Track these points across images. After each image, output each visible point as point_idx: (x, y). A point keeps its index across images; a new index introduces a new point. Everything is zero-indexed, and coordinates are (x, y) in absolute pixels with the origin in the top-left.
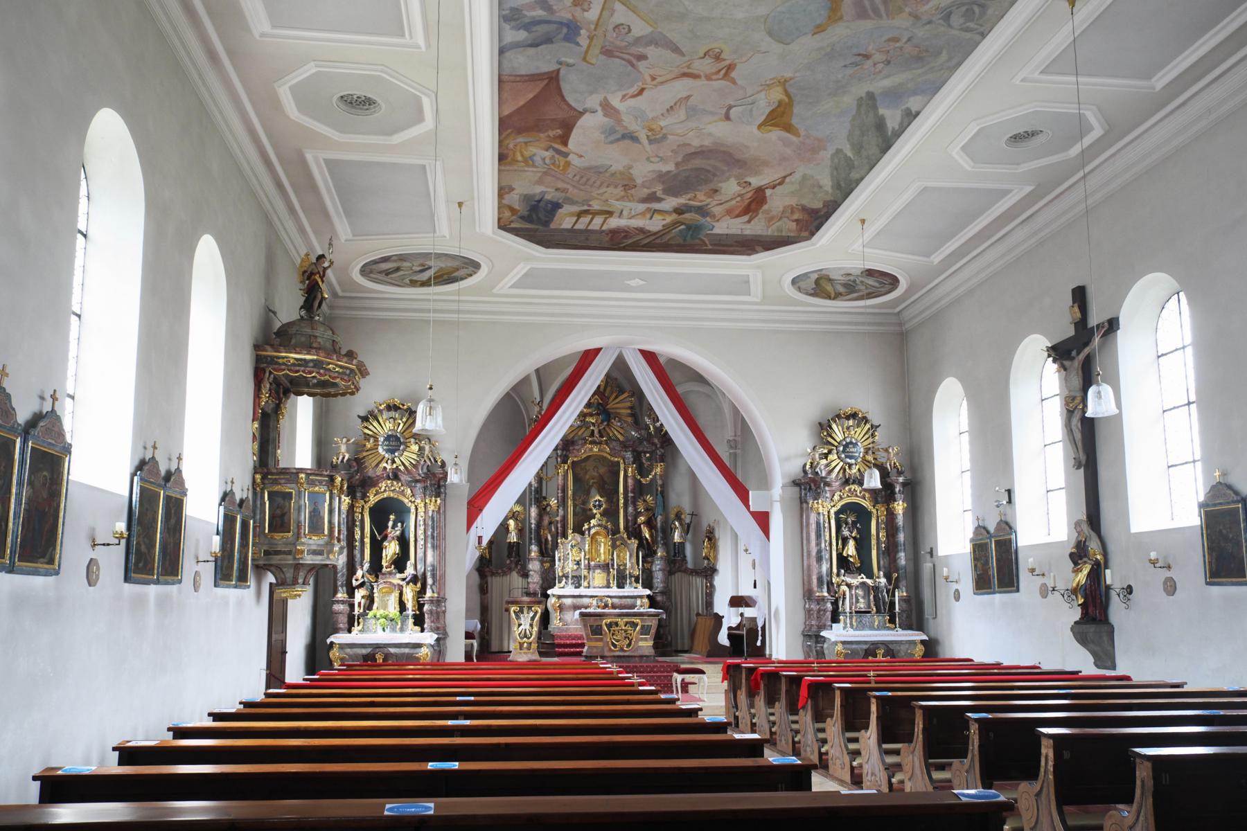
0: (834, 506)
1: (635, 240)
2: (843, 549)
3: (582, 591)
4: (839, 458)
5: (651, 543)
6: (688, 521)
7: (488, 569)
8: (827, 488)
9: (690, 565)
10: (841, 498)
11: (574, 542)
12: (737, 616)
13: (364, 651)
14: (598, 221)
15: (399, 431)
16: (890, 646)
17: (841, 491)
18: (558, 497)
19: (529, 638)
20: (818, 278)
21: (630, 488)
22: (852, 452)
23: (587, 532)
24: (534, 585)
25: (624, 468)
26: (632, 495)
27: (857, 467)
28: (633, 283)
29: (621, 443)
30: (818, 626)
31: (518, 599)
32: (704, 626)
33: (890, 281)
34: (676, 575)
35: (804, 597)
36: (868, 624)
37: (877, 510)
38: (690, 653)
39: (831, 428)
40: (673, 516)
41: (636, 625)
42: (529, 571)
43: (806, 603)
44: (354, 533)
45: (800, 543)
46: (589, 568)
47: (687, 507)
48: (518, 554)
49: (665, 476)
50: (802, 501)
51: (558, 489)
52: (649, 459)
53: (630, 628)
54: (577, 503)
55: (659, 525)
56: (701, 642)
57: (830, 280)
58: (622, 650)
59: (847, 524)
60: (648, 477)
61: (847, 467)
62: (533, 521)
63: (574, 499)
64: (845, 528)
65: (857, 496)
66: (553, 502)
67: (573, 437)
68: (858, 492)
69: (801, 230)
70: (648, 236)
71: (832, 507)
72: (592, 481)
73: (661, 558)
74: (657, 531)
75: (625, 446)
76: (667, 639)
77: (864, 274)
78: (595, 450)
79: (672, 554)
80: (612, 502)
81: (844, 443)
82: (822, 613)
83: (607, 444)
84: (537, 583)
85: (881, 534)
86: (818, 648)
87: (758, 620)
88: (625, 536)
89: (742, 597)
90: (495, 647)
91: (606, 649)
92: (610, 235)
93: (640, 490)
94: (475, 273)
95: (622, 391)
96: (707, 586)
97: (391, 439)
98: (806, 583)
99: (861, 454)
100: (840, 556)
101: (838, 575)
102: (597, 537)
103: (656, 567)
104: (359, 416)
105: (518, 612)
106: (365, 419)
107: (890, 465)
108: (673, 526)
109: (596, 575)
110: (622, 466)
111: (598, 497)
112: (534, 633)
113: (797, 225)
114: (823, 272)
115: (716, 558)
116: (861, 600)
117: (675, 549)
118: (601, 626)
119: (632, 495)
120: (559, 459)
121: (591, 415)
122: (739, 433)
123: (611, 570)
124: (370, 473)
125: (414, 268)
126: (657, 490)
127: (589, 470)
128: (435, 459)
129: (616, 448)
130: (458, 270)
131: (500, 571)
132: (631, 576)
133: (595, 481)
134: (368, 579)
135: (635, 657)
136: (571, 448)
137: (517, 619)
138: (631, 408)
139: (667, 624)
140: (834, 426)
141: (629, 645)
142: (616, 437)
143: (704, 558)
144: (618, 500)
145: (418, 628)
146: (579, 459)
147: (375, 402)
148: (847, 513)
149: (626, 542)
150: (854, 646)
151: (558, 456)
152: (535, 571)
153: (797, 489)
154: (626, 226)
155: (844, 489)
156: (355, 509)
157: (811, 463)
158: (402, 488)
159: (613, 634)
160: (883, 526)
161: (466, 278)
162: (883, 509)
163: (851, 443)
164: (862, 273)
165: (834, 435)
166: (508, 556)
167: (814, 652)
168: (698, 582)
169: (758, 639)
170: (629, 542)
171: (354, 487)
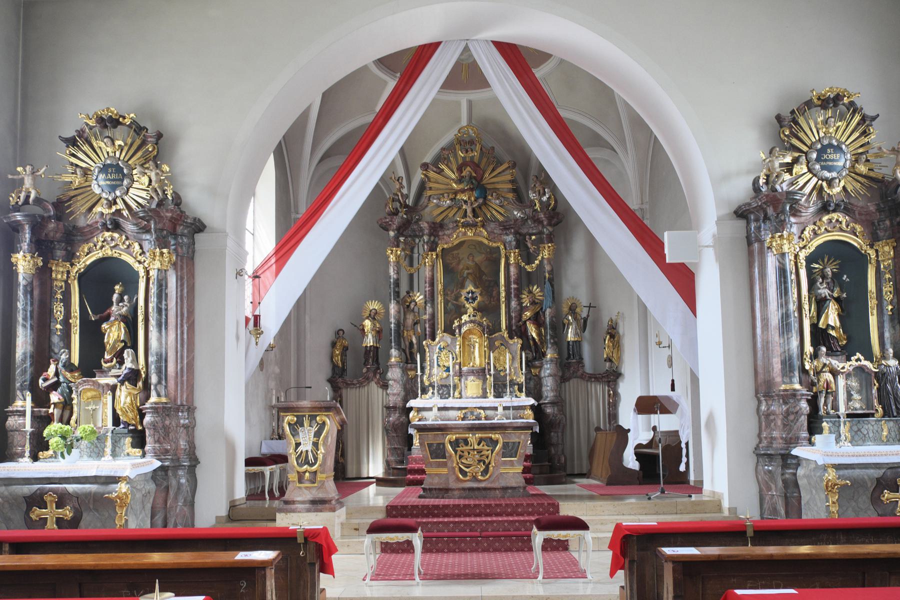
0: (804, 247)
2: (819, 317)
3: (450, 402)
4: (810, 170)
5: (539, 343)
6: (584, 315)
7: (340, 380)
8: (793, 220)
9: (588, 367)
10: (816, 234)
11: (442, 344)
12: (649, 431)
13: (27, 489)
15: (122, 158)
17: (815, 224)
18: (426, 292)
19: (312, 465)
21: (513, 278)
22: (833, 160)
23: (457, 331)
24: (395, 398)
25: (505, 255)
26: (516, 286)
27: (842, 183)
29: (501, 224)
30: (785, 439)
31: (295, 404)
32: (605, 444)
34: (571, 381)
35: (757, 392)
36: (871, 435)
37: (877, 251)
38: (588, 478)
39: (796, 123)
40: (565, 309)
41: (496, 442)
42: (389, 381)
43: (760, 402)
45: (748, 305)
46: (460, 374)
47: (583, 298)
48: (376, 360)
49: (557, 261)
50: (750, 240)
51: (426, 283)
52: (533, 242)
53: (486, 447)
54: (449, 298)
55: (548, 320)
56: (601, 465)
58: (475, 479)
59: (824, 277)
60: (534, 263)
61: (824, 184)
62: (392, 320)
63: (445, 295)
65: (841, 230)
66: (419, 298)
67: (443, 219)
68: (844, 223)
71: (801, 249)
72: (466, 272)
73: (551, 360)
74: (545, 329)
75: (505, 227)
76: (559, 460)
78: (470, 234)
79: (566, 355)
80: (491, 296)
81: (819, 146)
82: (792, 417)
83: (483, 226)
84: (399, 395)
85: (884, 290)
86: (787, 476)
87: (681, 434)
88: (506, 335)
89: (655, 397)
90: (351, 472)
91: (452, 479)
93: (525, 280)
95: (500, 163)
96: (609, 395)
97: (110, 170)
98: (760, 370)
99: (848, 163)
100: (814, 327)
101: (815, 356)
102: (471, 336)
103: (545, 372)
105: (296, 423)
106: (72, 142)
108: (566, 321)
109: (468, 382)
110: (503, 252)
111: (471, 288)
115: (620, 358)
116: (856, 396)
117: (569, 350)
118: (444, 444)
119: (516, 286)
120: (426, 247)
121: (463, 191)
122: (647, 199)
123: (488, 376)
124: (82, 223)
126: (545, 277)
127: (463, 258)
128: (164, 191)
129: (495, 231)
131: (355, 382)
132: (512, 383)
133: (470, 271)
134: (65, 377)
135: (495, 489)
137: (293, 436)
138: (512, 182)
139: (560, 442)
140: (801, 120)
141: (486, 471)
142: (495, 218)
143: (605, 360)
144: (499, 293)
145: (138, 452)
146: (450, 245)
148: (823, 261)
149: (507, 342)
150: (857, 472)
151: (424, 242)
152: (395, 380)
153: (742, 223)
155: (820, 220)
156: (54, 275)
157: (768, 176)
158: (127, 243)
159: (461, 457)
160: (888, 276)
162: (887, 249)
163: (830, 145)
165: (801, 135)
166: (364, 364)
167: (780, 483)
168: (599, 390)
169: (681, 462)
170: (511, 342)
171: (52, 242)
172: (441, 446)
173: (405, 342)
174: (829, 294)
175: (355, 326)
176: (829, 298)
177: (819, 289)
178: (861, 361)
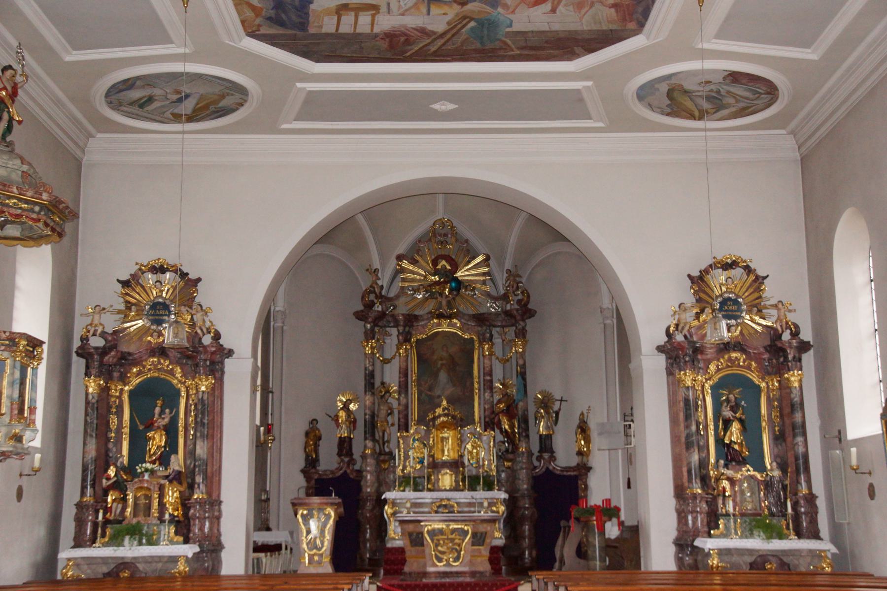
0: (710, 379)
1: (421, 45)
6: (556, 408)
14: (365, 19)
16: (785, 559)
17: (718, 360)
19: (320, 549)
20: (669, 90)
28: (440, 106)
33: (764, 89)
44: (108, 422)
53: (458, 537)
54: (422, 389)
57: (686, 92)
63: (419, 385)
64: (726, 406)
69: (624, 20)
70: (435, 39)
71: (707, 380)
72: (440, 362)
77: (727, 81)
92: (387, 40)
94: (246, 101)
97: (158, 307)
104: (118, 281)
107: (781, 326)
112: (326, 543)
113: (617, 11)
114: (673, 81)
118: (422, 533)
120: (400, 338)
125: (169, 96)
130: (223, 97)
133: (444, 362)
136: (415, 324)
147: (137, 264)
154: (401, 26)
161: (237, 109)
164: (724, 78)
172: (420, 536)
173: (379, 434)
174: (732, 415)
175: (330, 417)
176: (732, 418)
177: (724, 411)
178: (750, 471)
